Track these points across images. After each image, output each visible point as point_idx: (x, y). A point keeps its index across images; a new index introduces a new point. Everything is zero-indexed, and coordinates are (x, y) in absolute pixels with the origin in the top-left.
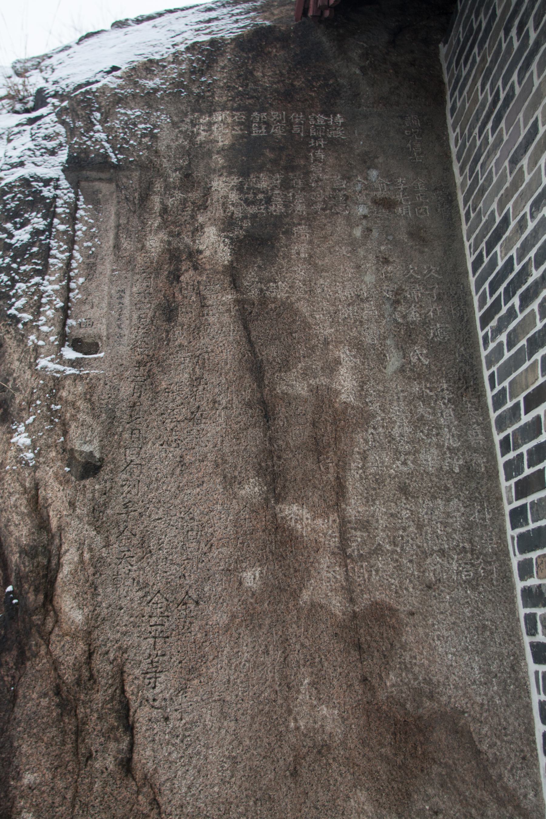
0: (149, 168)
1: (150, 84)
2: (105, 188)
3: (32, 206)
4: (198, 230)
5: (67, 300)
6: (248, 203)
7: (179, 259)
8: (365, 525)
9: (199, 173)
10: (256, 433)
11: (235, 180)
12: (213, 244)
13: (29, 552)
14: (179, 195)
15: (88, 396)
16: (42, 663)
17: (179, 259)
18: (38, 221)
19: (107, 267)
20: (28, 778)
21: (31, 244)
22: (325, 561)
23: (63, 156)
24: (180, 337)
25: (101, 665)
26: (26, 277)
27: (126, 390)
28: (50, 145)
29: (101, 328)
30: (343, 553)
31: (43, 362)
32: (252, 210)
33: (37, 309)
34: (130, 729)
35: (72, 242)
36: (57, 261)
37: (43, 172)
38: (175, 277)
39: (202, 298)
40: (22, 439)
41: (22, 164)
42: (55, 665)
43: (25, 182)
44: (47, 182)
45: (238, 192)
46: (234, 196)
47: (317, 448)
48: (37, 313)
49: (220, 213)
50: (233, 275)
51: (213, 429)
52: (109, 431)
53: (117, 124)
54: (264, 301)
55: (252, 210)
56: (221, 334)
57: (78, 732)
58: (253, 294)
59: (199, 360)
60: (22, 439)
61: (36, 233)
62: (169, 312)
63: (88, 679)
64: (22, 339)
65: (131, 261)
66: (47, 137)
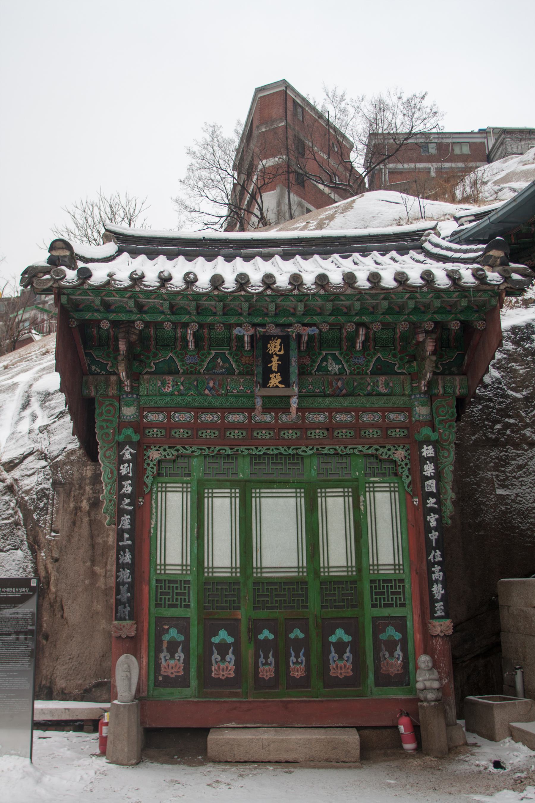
0: (71, 484)
1: (72, 458)
2: (61, 490)
3: (44, 496)
4: (82, 501)
5: (52, 521)
6: (94, 493)
7: (77, 509)
8: (110, 571)
9: (83, 485)
10: (90, 551)
11: (91, 487)
12: (85, 505)
13: (45, 578)
14: (78, 491)
15: (56, 544)
16: (47, 599)
17: (77, 509)
18: (45, 501)
19: (61, 511)
20: (45, 619)
21: (43, 507)
22: (102, 578)
23: (51, 481)
24: (76, 529)
25: (58, 599)
26: (43, 516)
27: (64, 543)
28: (48, 477)
29: (60, 527)
30: (105, 577)
31: (47, 537)
32: (95, 495)
33: (45, 523)
34: (63, 610)
35: (53, 505)
36: (50, 509)
37: (47, 486)
38: (76, 514)
39: (82, 519)
40: (43, 554)
41: (41, 484)
42: (50, 599)
43: (42, 490)
44: (47, 489)
45: (149, 450)
46: (91, 491)
47: (103, 555)
48: (46, 525)
49: (87, 496)
50: (89, 513)
51: (82, 551)
52: (60, 552)
53: (64, 471)
54: (95, 520)
55: (95, 495)
56: (85, 529)
57: (54, 611)
58: (93, 518)
59: (80, 535)
60: (43, 554)
61: (45, 504)
62: (74, 523)
63: (55, 601)
64: (42, 531)
65: (66, 510)
66: (47, 475)
